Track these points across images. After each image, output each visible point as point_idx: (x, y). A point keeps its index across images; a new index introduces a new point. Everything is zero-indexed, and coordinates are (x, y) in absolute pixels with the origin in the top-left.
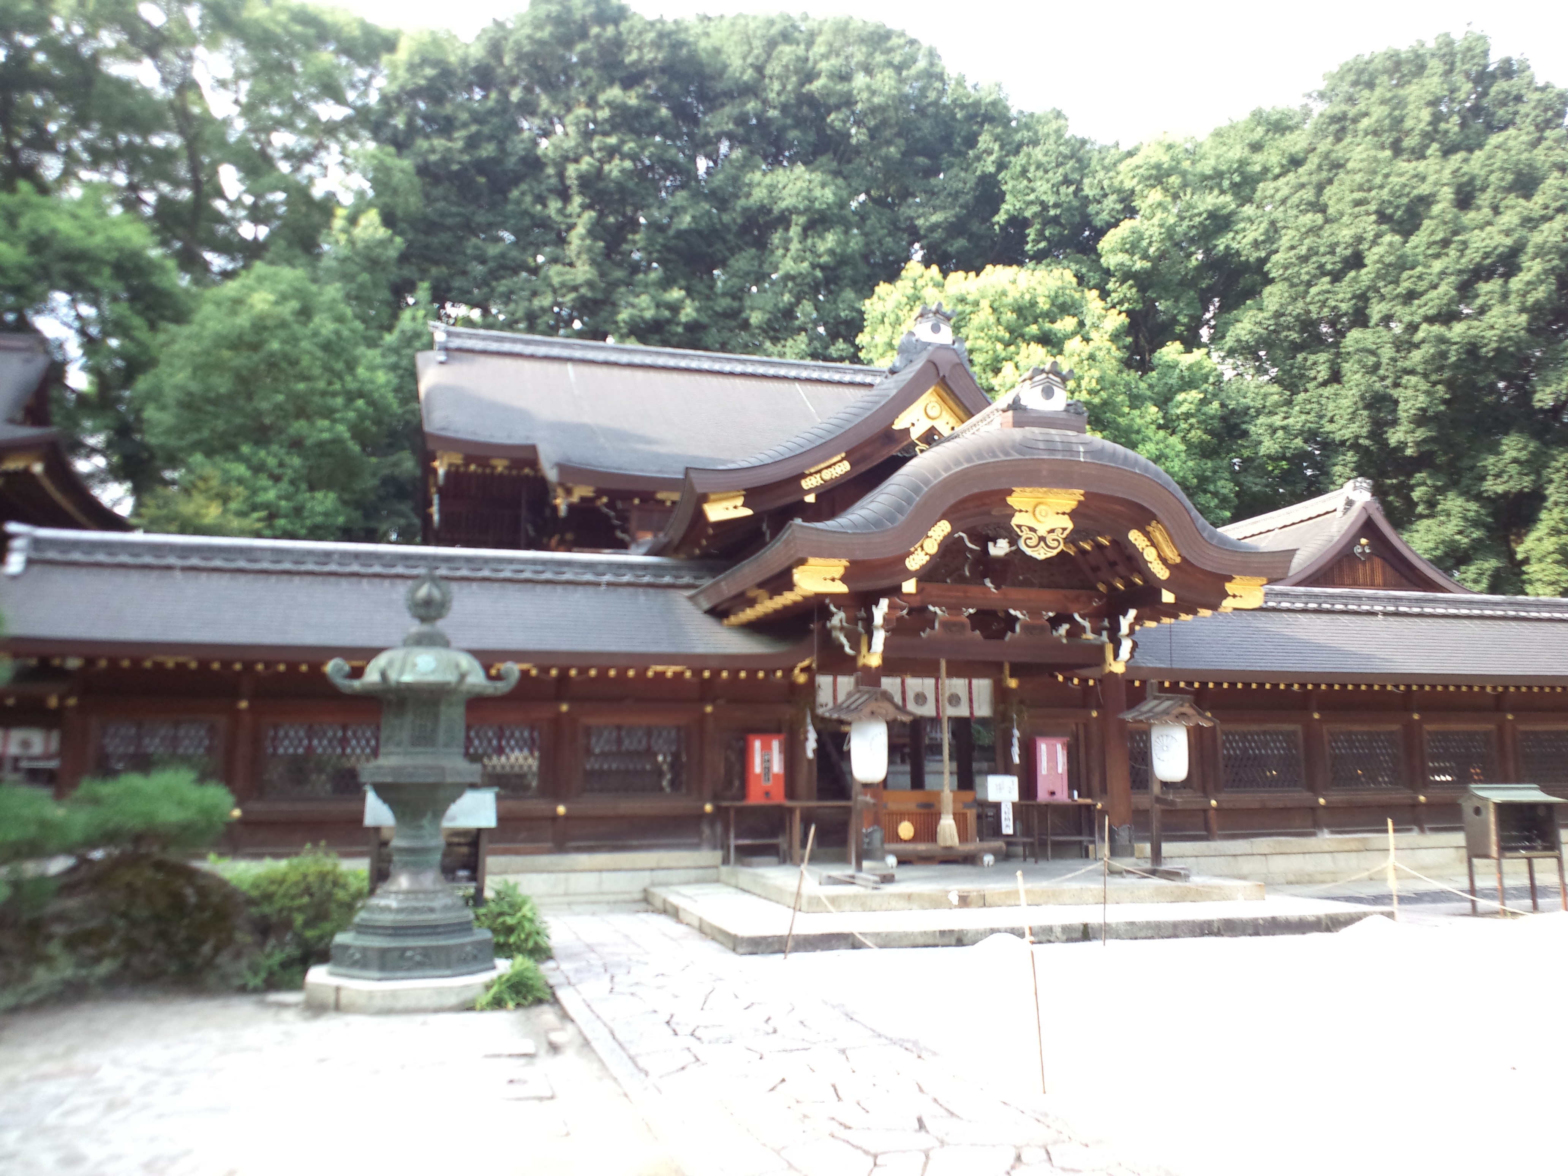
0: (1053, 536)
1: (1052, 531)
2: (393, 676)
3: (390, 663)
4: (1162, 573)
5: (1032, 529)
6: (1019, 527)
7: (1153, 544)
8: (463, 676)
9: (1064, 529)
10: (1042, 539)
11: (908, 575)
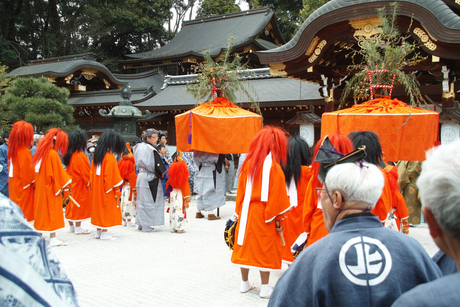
0: (374, 38)
1: (373, 36)
2: (115, 113)
3: (114, 110)
4: (431, 47)
6: (357, 37)
7: (313, 52)
8: (133, 114)
9: (378, 34)
11: (309, 65)
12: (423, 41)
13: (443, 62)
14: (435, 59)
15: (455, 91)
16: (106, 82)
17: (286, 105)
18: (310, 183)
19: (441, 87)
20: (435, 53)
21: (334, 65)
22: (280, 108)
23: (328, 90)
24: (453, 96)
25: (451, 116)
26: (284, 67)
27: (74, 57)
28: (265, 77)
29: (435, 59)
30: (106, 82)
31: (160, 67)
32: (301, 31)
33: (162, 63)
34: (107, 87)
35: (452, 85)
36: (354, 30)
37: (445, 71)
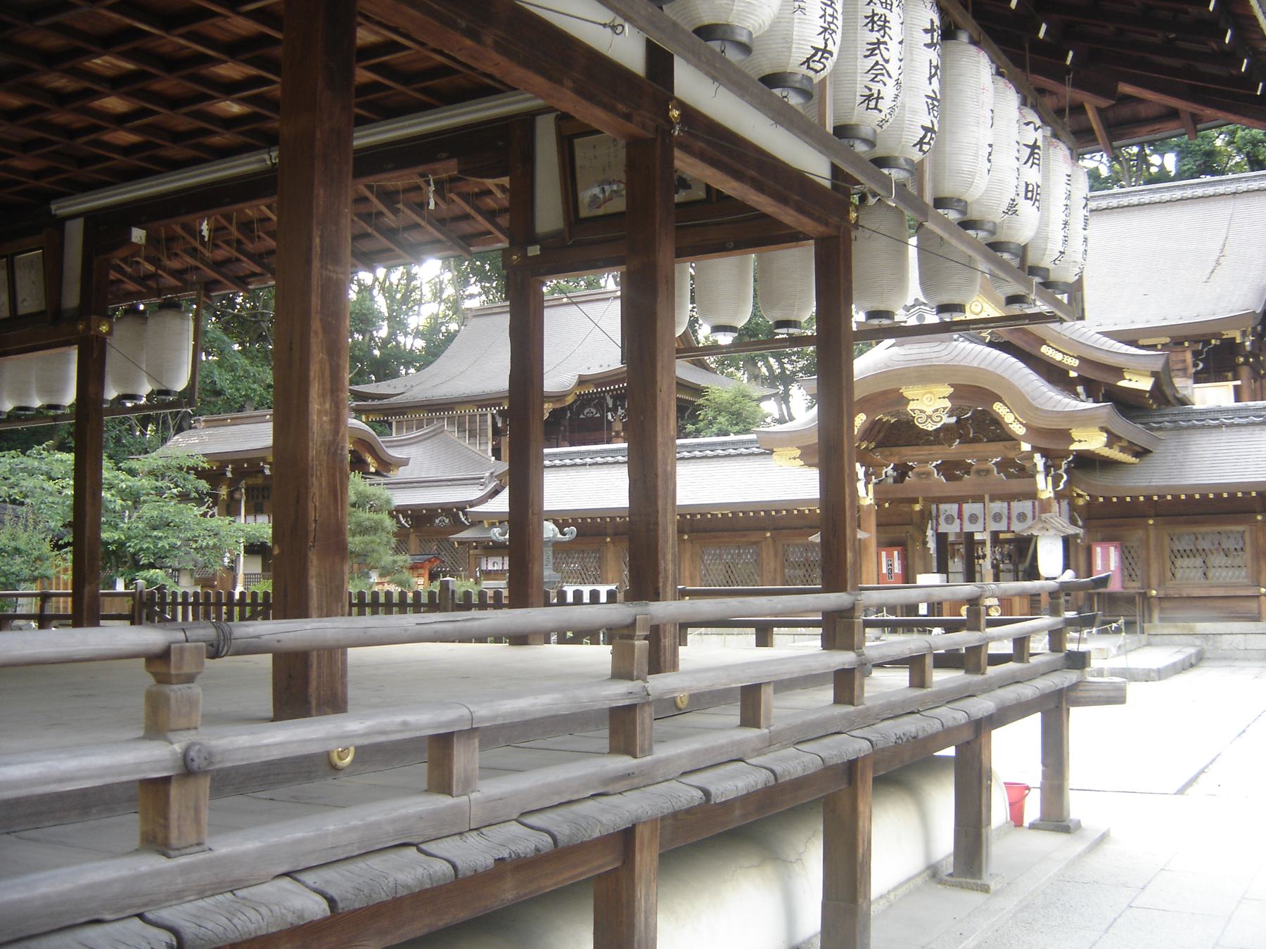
4: (1019, 430)
5: (922, 411)
10: (929, 417)
12: (1007, 421)
13: (1035, 449)
14: (1026, 447)
15: (1054, 488)
16: (369, 459)
17: (692, 512)
18: (954, 242)
19: (1035, 483)
20: (1025, 438)
21: (872, 445)
22: (693, 515)
23: (867, 484)
24: (1052, 495)
25: (1047, 526)
26: (798, 452)
27: (665, 471)
28: (726, 453)
29: (1026, 447)
30: (369, 459)
31: (451, 420)
32: (860, 547)
33: (453, 409)
34: (372, 470)
35: (1050, 479)
36: (907, 401)
37: (1039, 460)
